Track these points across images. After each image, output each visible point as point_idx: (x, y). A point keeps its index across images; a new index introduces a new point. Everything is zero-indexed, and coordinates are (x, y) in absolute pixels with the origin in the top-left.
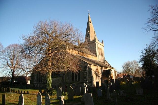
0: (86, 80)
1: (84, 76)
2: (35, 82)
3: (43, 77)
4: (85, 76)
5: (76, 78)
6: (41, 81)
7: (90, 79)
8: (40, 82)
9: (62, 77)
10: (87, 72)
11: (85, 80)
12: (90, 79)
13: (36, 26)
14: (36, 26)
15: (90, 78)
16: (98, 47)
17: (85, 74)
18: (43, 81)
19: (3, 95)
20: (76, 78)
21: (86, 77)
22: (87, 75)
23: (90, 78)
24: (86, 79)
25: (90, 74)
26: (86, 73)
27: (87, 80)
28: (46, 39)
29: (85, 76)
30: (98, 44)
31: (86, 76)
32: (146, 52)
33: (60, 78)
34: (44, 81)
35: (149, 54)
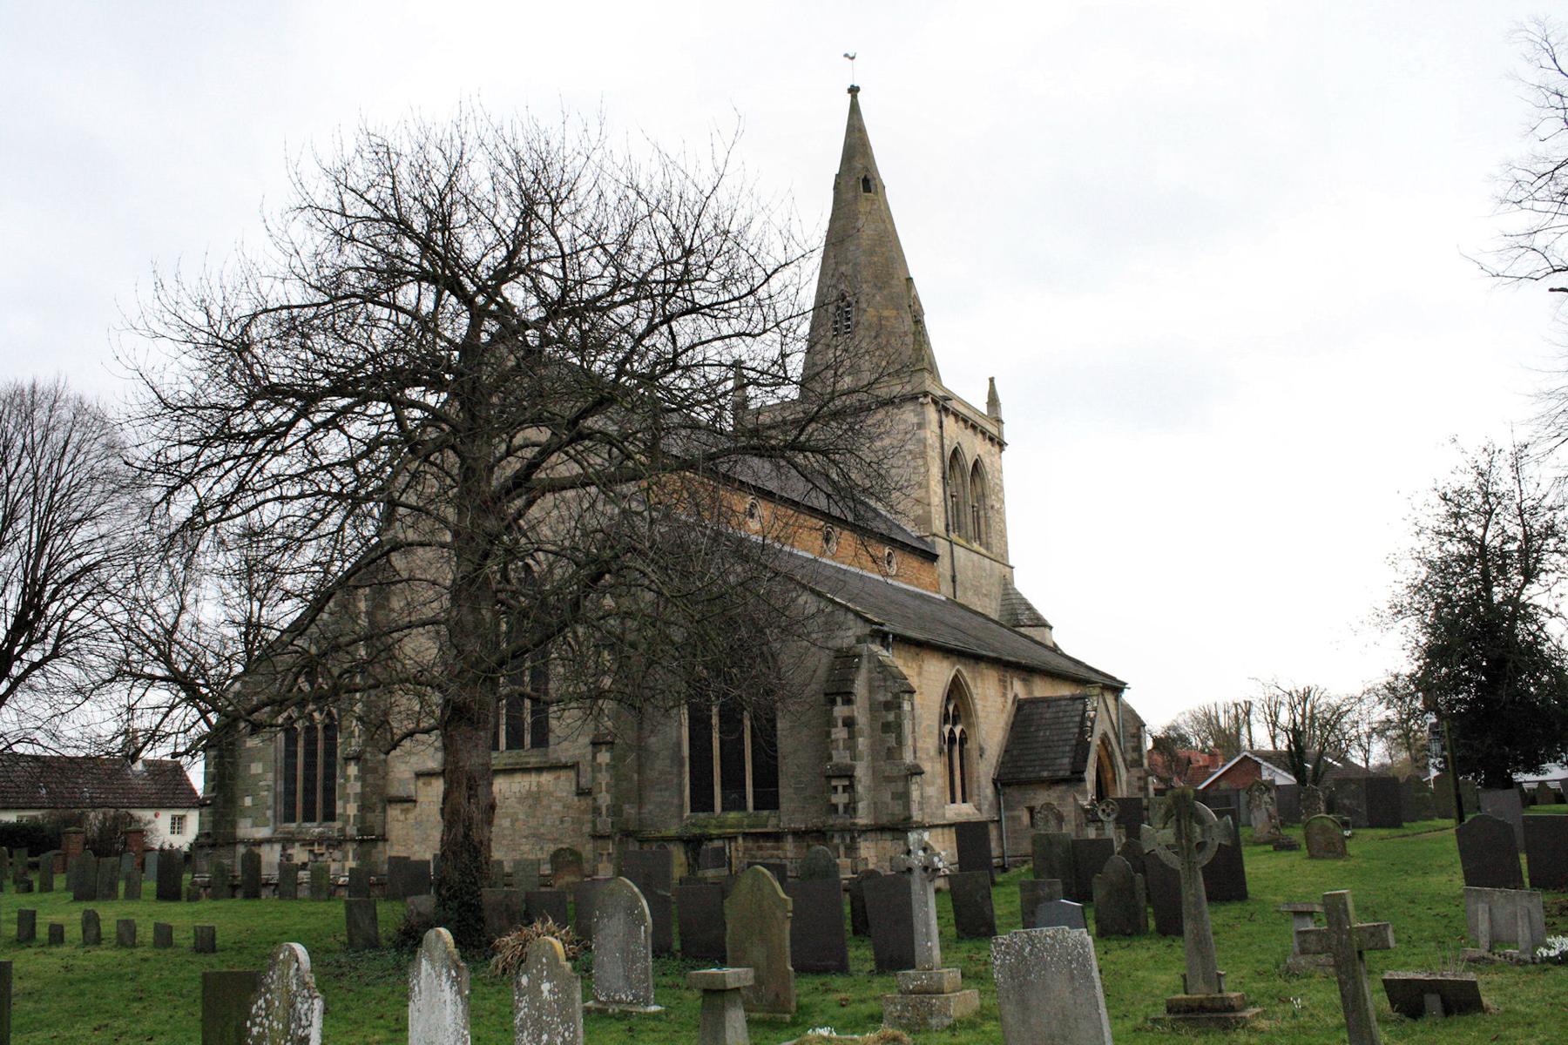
0: (851, 808)
1: (830, 758)
2: (255, 825)
3: (353, 770)
4: (840, 757)
5: (733, 781)
6: (330, 816)
7: (896, 796)
8: (315, 829)
9: (574, 766)
10: (862, 720)
11: (840, 799)
12: (888, 797)
13: (324, 194)
14: (324, 194)
15: (889, 779)
16: (948, 453)
17: (840, 733)
18: (352, 809)
19: (86, 912)
20: (733, 781)
21: (848, 774)
22: (862, 743)
23: (889, 779)
24: (849, 789)
25: (892, 742)
26: (849, 723)
27: (860, 805)
28: (316, 376)
29: (840, 757)
30: (949, 422)
31: (848, 761)
32: (1457, 516)
33: (546, 778)
34: (362, 808)
35: (1483, 547)
